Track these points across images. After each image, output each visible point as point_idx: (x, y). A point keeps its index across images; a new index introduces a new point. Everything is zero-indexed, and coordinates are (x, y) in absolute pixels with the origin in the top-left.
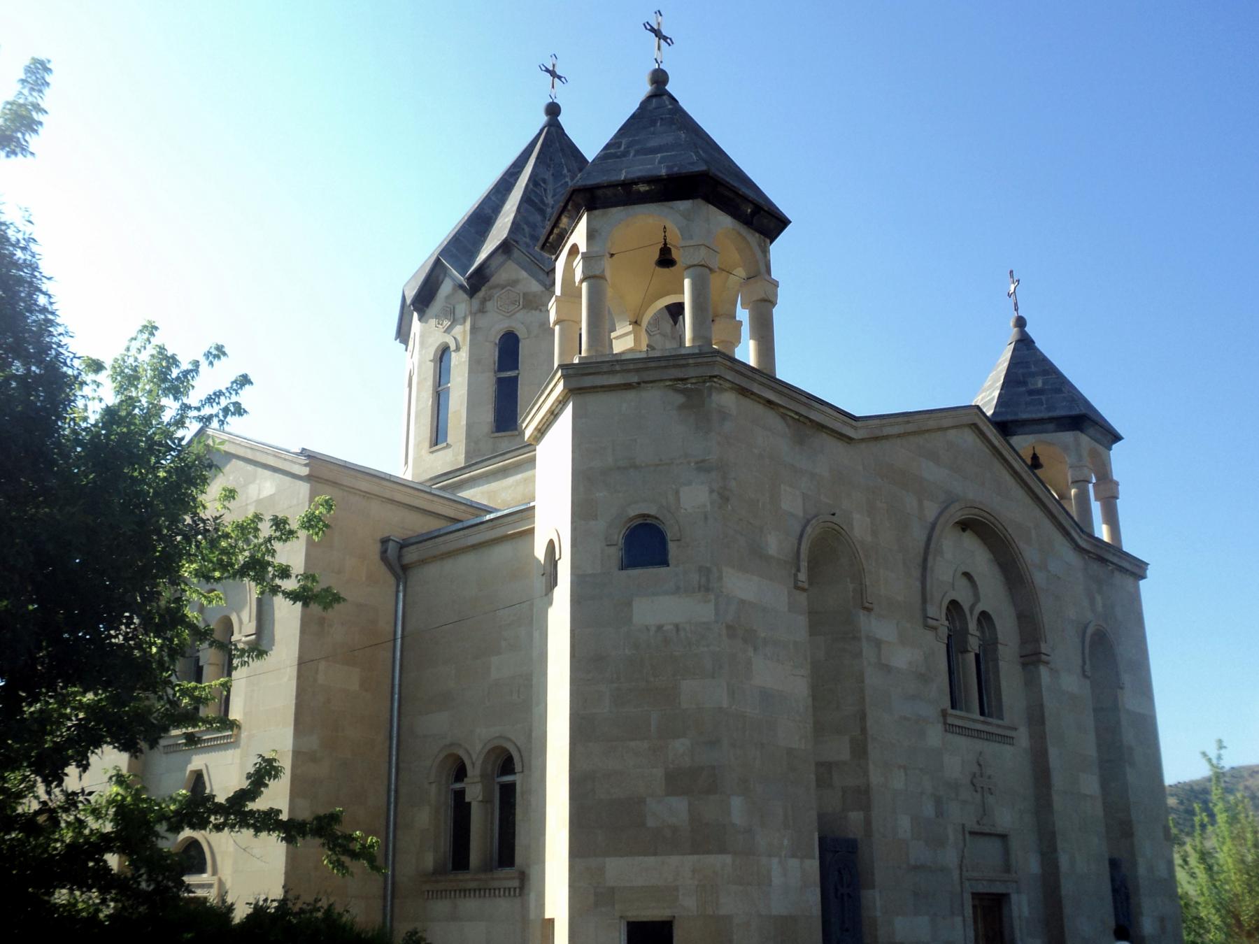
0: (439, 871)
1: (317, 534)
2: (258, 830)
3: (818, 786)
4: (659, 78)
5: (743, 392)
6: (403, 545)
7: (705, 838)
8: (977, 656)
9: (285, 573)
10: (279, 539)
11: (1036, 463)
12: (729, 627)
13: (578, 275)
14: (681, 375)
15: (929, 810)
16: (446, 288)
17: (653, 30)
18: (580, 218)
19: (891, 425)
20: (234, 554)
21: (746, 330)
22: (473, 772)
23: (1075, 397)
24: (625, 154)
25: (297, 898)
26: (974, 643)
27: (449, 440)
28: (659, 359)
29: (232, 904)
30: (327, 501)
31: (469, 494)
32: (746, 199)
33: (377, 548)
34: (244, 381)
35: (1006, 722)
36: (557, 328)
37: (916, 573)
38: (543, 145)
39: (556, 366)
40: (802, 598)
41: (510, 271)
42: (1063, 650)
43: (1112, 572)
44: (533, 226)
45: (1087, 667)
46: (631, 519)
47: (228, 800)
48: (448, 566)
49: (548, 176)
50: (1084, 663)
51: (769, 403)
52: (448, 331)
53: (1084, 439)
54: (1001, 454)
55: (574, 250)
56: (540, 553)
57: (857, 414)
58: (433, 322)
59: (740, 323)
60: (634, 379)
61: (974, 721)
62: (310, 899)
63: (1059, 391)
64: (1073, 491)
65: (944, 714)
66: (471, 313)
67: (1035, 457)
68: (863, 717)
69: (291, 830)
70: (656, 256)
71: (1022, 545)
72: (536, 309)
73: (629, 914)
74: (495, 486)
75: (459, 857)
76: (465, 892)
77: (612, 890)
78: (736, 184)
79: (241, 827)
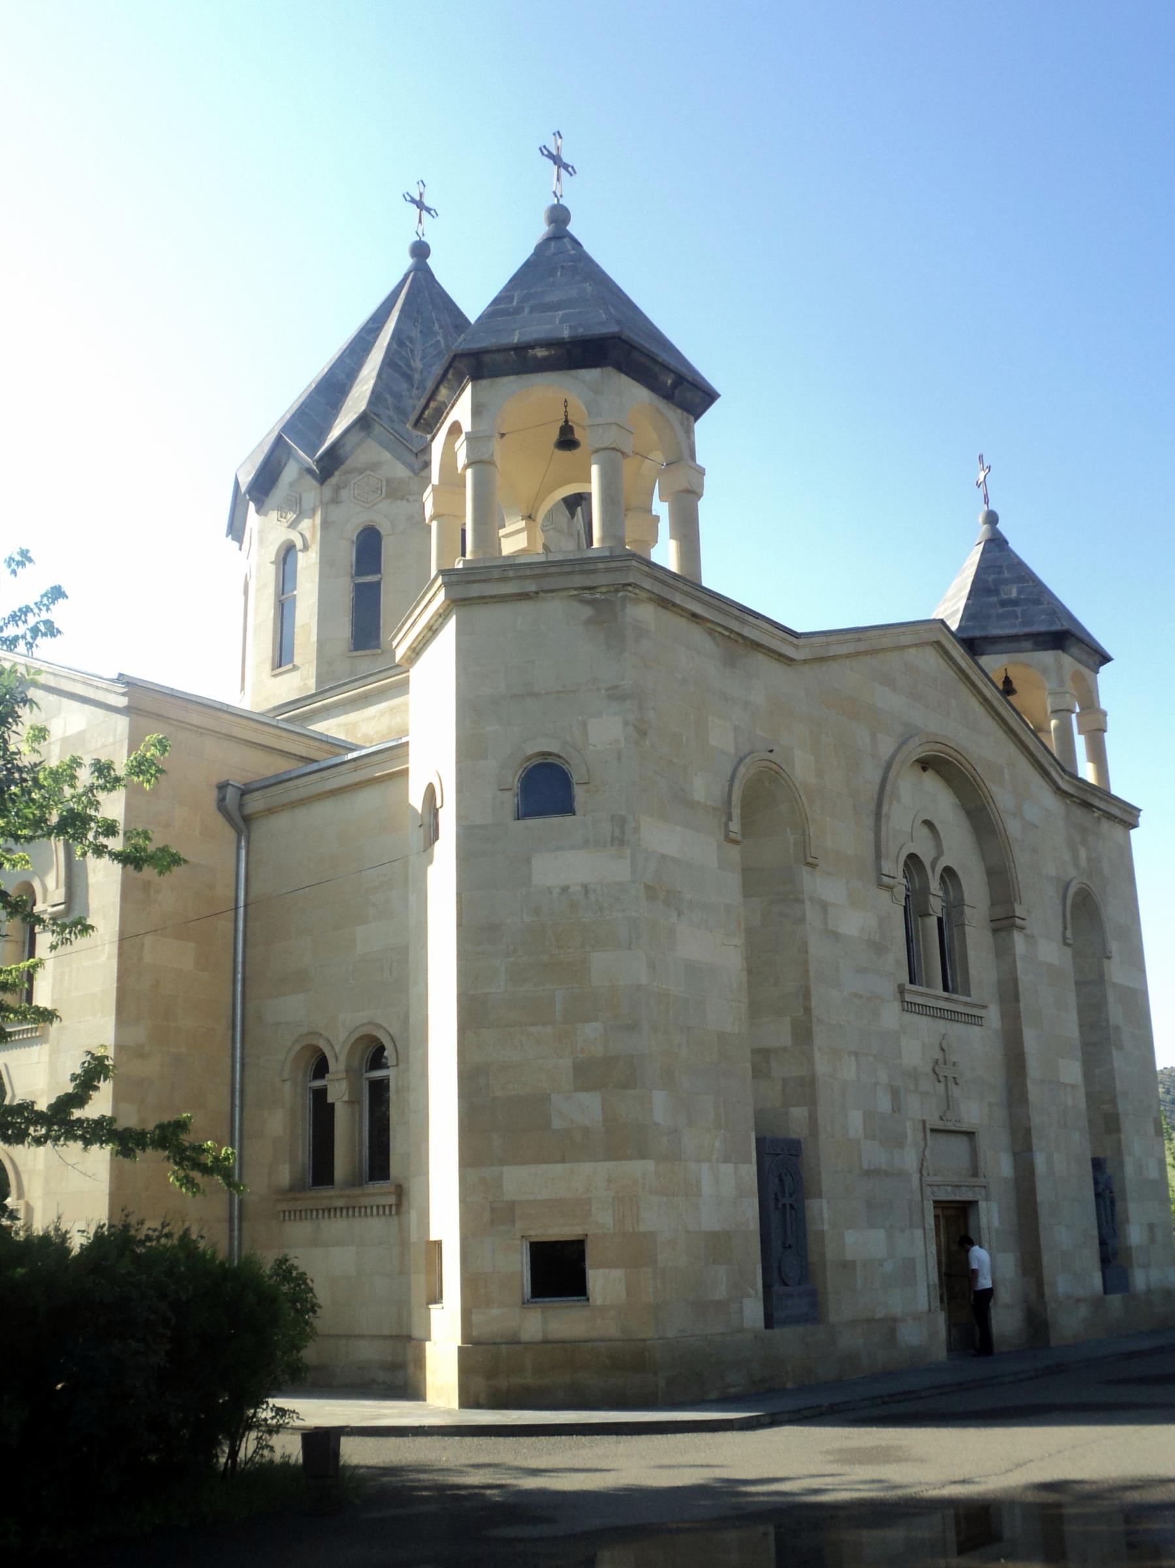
0: (296, 1188)
1: (149, 781)
2: (87, 1143)
3: (754, 1077)
4: (559, 216)
5: (664, 603)
6: (245, 792)
7: (621, 1141)
8: (940, 920)
9: (110, 829)
10: (103, 788)
11: (1008, 688)
12: (647, 887)
13: (462, 459)
14: (589, 584)
15: (884, 1104)
16: (290, 473)
17: (550, 156)
18: (463, 390)
19: (839, 643)
20: (47, 807)
21: (664, 527)
22: (336, 1067)
23: (1057, 609)
24: (518, 310)
25: (141, 1223)
26: (936, 905)
27: (297, 660)
28: (561, 563)
29: (67, 1232)
30: (160, 741)
31: (322, 727)
32: (666, 368)
33: (213, 795)
34: (57, 593)
35: (974, 998)
36: (434, 525)
37: (869, 821)
38: (408, 294)
39: (434, 572)
40: (734, 853)
41: (370, 452)
42: (1040, 910)
43: (1099, 819)
44: (398, 397)
45: (1069, 934)
46: (529, 758)
47: (50, 1107)
48: (303, 816)
49: (415, 333)
50: (1065, 928)
51: (695, 616)
52: (293, 525)
53: (1066, 659)
54: (967, 677)
55: (456, 428)
56: (416, 800)
57: (799, 630)
58: (274, 515)
59: (657, 518)
60: (531, 587)
61: (937, 997)
62: (156, 1224)
63: (1037, 602)
64: (1053, 723)
65: (902, 990)
66: (321, 503)
67: (1007, 681)
68: (807, 995)
69: (123, 1140)
70: (555, 435)
71: (995, 789)
72: (402, 498)
73: (532, 1233)
74: (353, 717)
75: (321, 1169)
76: (330, 1211)
77: (512, 1205)
78: (655, 350)
79: (66, 1139)
